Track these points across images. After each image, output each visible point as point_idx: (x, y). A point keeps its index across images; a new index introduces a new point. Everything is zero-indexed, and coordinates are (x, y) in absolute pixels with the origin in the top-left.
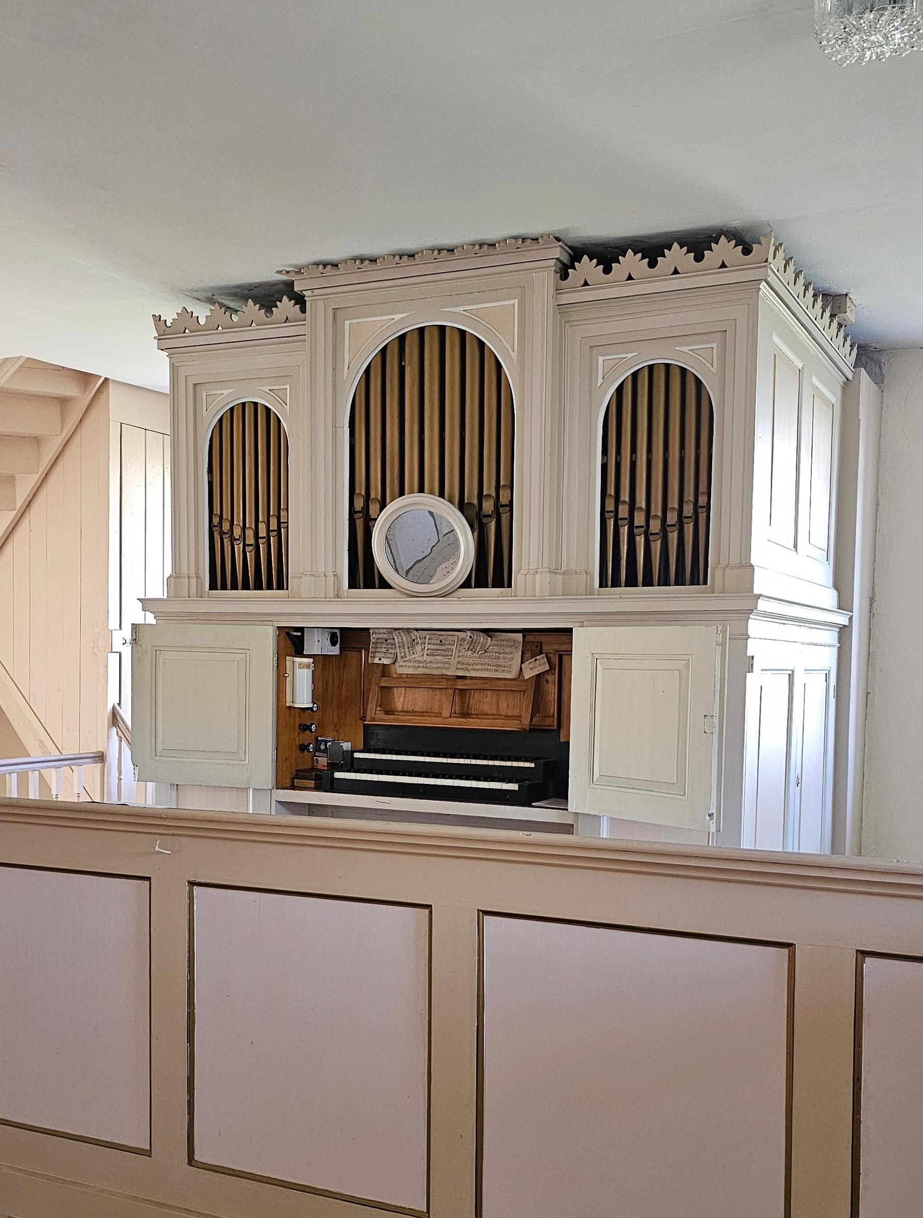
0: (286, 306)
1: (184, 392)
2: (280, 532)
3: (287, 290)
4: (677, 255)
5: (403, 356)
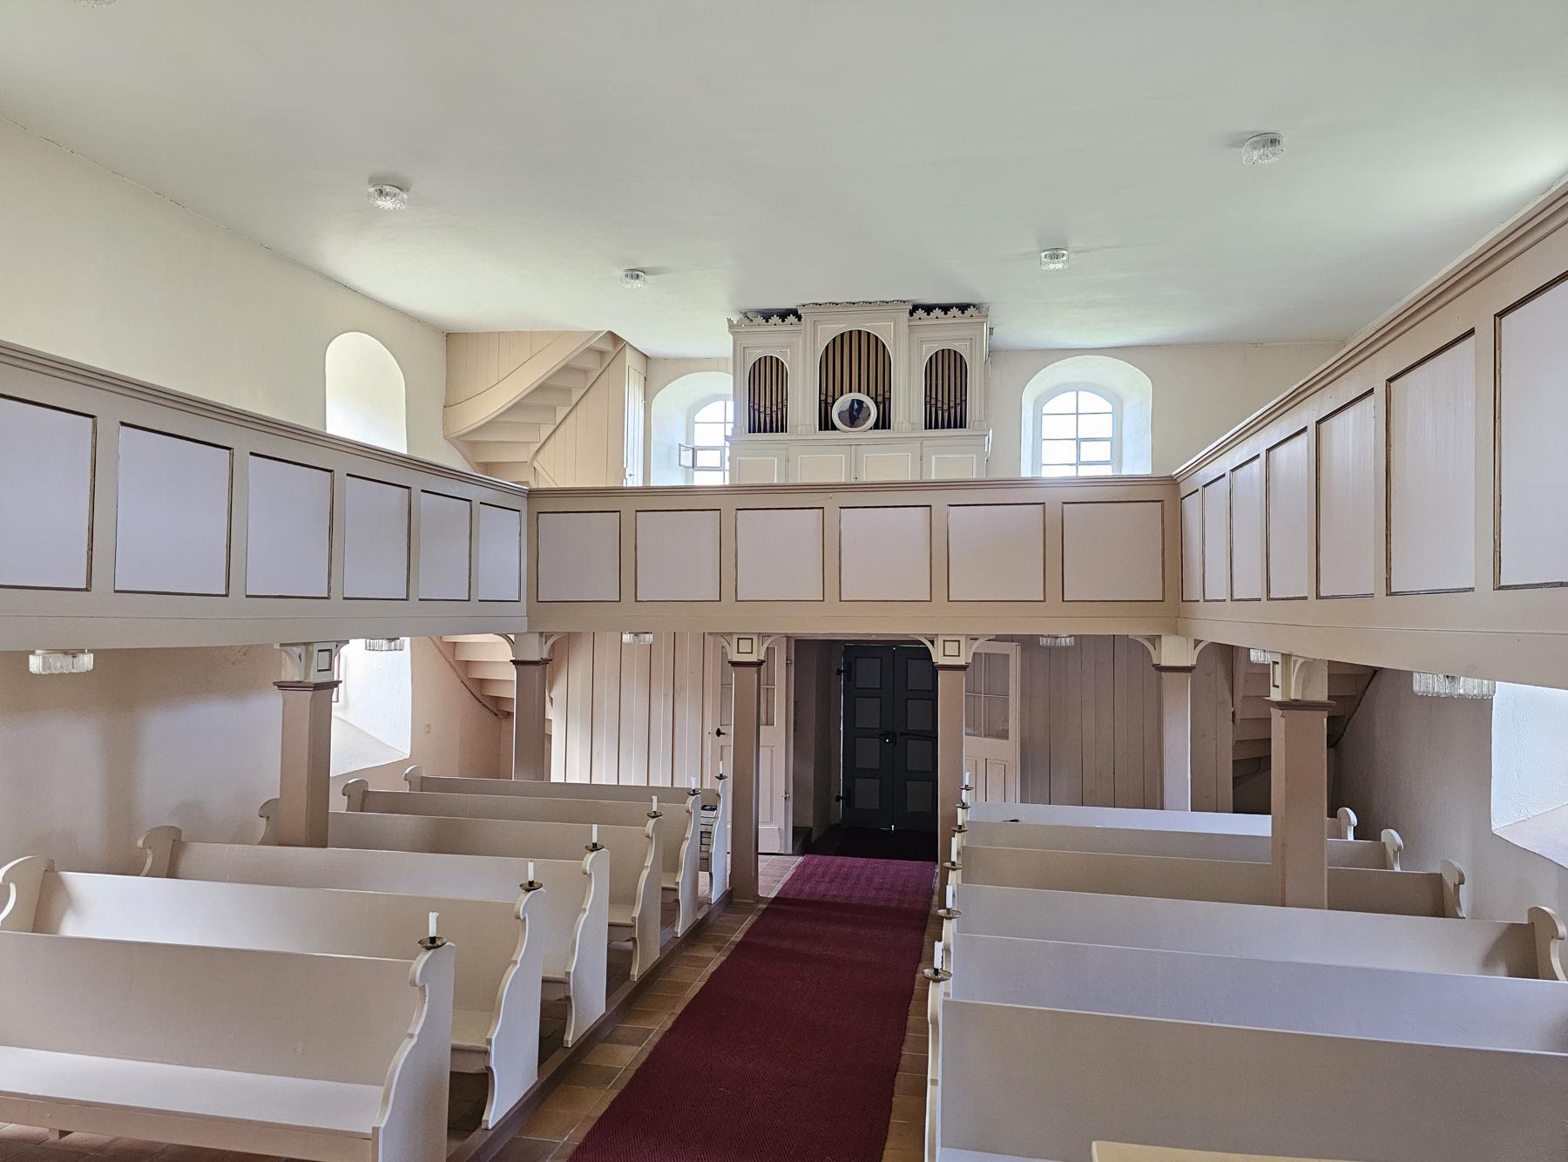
0: (791, 318)
1: (739, 350)
2: (783, 405)
3: (795, 313)
4: (954, 311)
5: (841, 342)
